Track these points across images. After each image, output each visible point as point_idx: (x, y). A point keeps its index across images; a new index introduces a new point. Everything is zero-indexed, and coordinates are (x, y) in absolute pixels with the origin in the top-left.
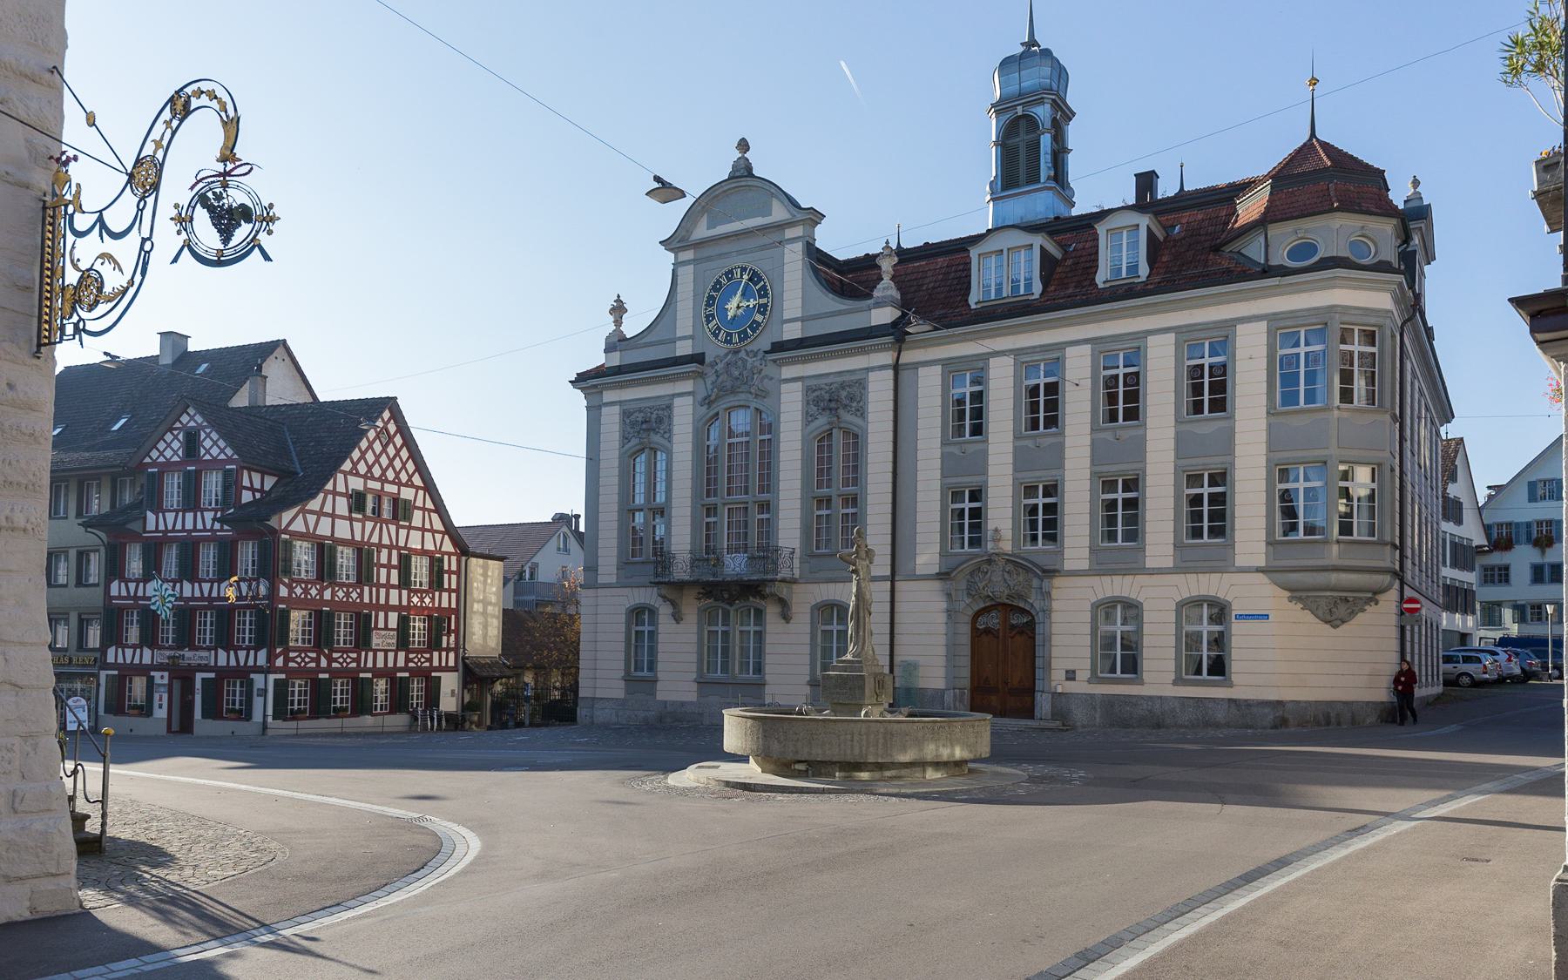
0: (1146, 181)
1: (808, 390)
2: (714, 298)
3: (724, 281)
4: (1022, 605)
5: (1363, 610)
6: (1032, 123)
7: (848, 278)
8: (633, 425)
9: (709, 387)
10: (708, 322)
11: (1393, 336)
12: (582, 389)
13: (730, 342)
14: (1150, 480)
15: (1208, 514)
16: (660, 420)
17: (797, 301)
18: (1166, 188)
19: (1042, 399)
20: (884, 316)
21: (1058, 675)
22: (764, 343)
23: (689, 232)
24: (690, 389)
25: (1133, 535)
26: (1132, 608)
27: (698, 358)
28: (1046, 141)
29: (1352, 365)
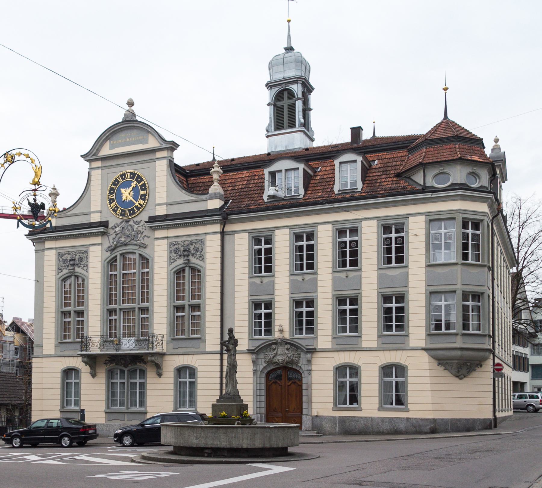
0: (356, 132)
1: (171, 244)
2: (114, 190)
3: (120, 180)
4: (294, 367)
5: (475, 370)
6: (291, 94)
7: (191, 178)
8: (64, 261)
9: (111, 241)
10: (110, 203)
11: (488, 226)
12: (32, 240)
13: (124, 215)
14: (364, 300)
15: (394, 316)
16: (81, 259)
17: (164, 194)
18: (366, 135)
19: (305, 253)
20: (215, 204)
22: (144, 217)
23: (98, 150)
24: (100, 242)
25: (355, 329)
26: (355, 370)
27: (105, 224)
28: (299, 105)
29: (468, 240)
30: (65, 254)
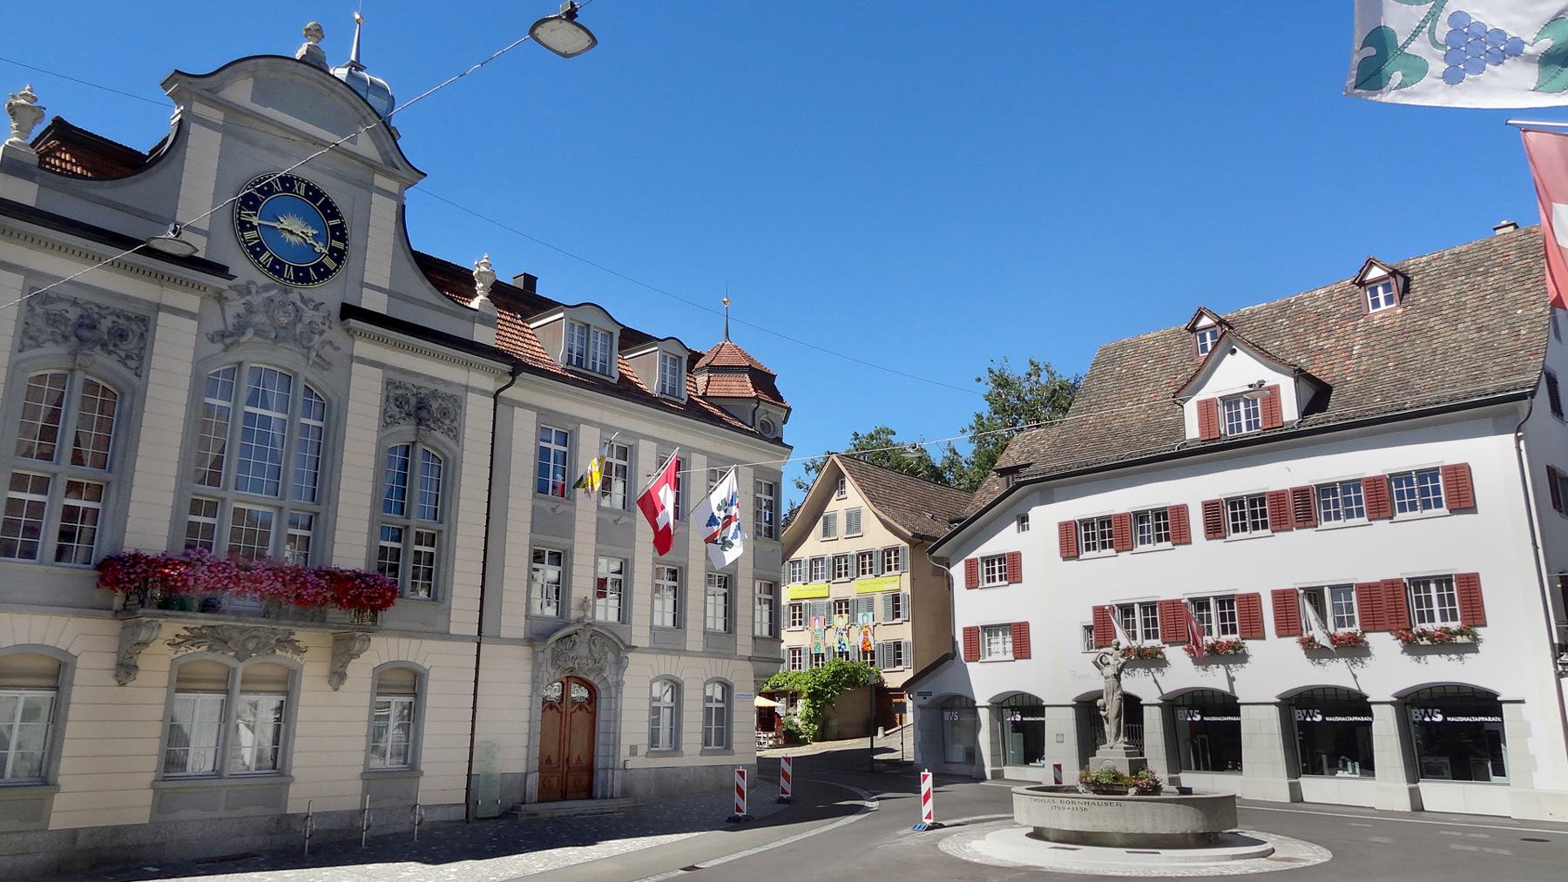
9: (230, 320)
21: (624, 752)
30: (61, 300)
